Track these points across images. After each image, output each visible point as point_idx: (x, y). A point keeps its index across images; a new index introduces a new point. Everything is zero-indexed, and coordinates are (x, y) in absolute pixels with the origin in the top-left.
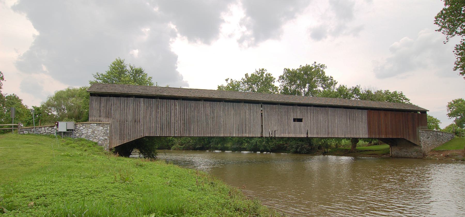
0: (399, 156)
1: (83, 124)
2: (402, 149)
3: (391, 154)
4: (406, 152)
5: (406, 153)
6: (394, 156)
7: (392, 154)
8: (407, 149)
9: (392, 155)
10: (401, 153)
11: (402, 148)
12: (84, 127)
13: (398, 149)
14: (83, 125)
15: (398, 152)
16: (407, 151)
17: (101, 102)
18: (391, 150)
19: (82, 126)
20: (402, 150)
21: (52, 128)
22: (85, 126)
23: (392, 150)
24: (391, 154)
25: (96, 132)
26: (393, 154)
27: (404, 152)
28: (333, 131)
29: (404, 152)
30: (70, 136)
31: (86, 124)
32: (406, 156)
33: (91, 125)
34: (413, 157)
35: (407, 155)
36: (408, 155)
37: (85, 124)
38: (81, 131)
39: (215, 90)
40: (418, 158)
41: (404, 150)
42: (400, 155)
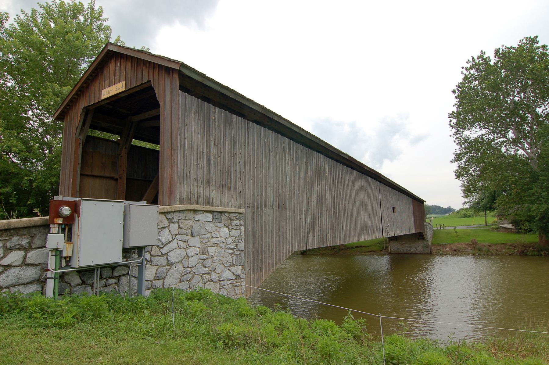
0: (400, 252)
1: (170, 216)
2: (404, 244)
3: (390, 250)
4: (409, 247)
5: (409, 249)
6: (394, 252)
7: (390, 249)
8: (410, 244)
9: (391, 251)
10: (403, 249)
11: (404, 242)
12: (174, 227)
13: (399, 244)
14: (170, 221)
15: (398, 247)
16: (410, 246)
17: (211, 124)
18: (390, 246)
19: (166, 223)
20: (404, 245)
21: (9, 244)
22: (176, 226)
23: (391, 245)
24: (390, 250)
25: (211, 250)
26: (392, 249)
27: (407, 247)
28: (269, 203)
29: (407, 247)
30: (117, 284)
31: (181, 215)
32: (410, 252)
33: (198, 217)
34: (419, 253)
35: (410, 250)
36: (412, 251)
37: (176, 216)
38: (164, 251)
39: (137, 48)
40: (425, 254)
41: (407, 245)
42: (402, 251)
